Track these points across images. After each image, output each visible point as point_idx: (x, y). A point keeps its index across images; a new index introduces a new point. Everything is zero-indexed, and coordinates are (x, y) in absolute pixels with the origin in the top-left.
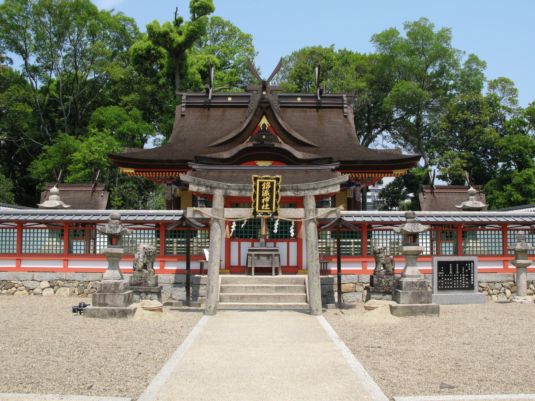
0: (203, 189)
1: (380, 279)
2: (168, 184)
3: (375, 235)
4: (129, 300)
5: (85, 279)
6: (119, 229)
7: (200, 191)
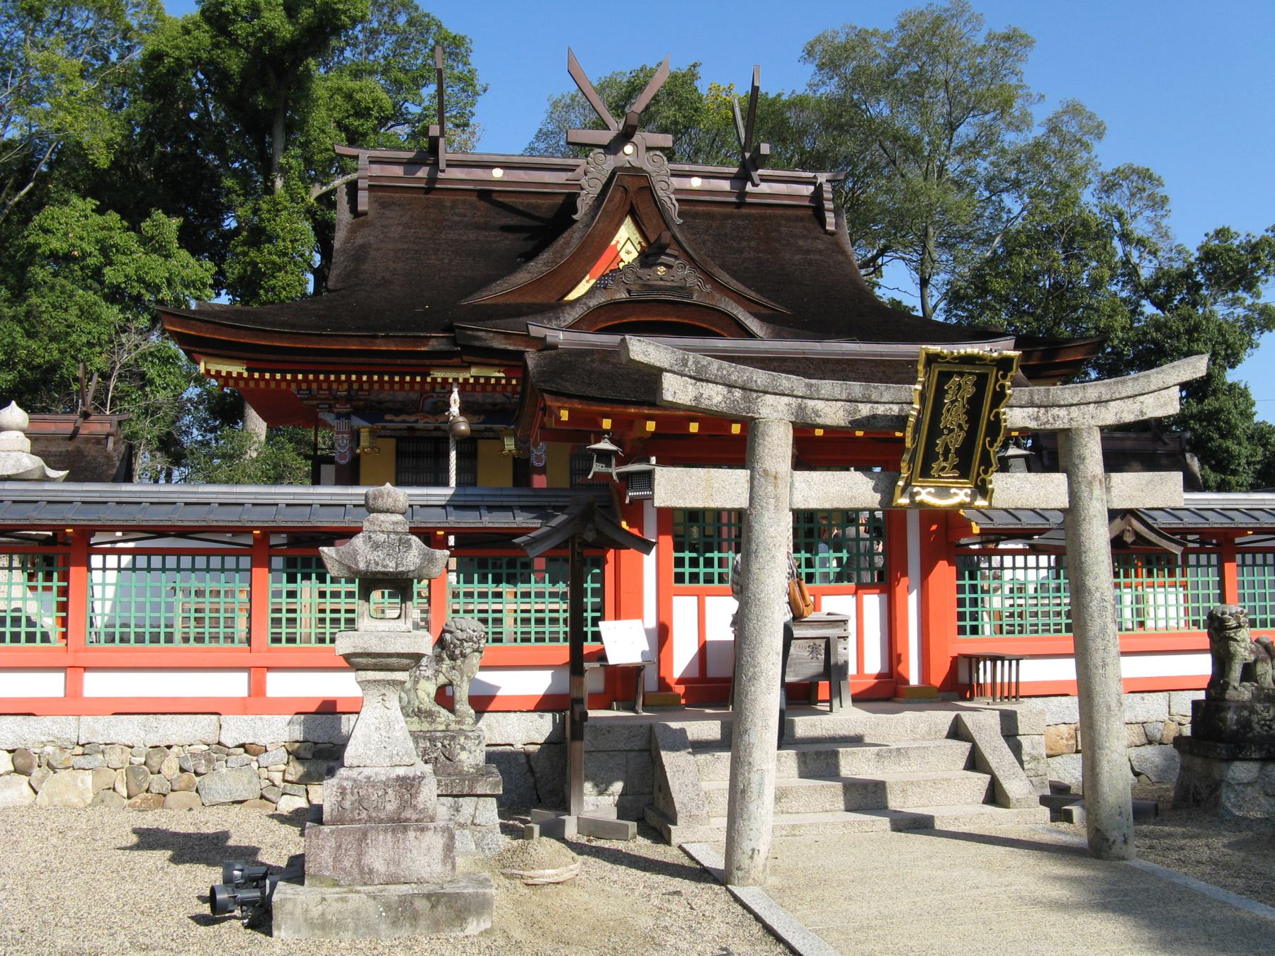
7: (705, 403)
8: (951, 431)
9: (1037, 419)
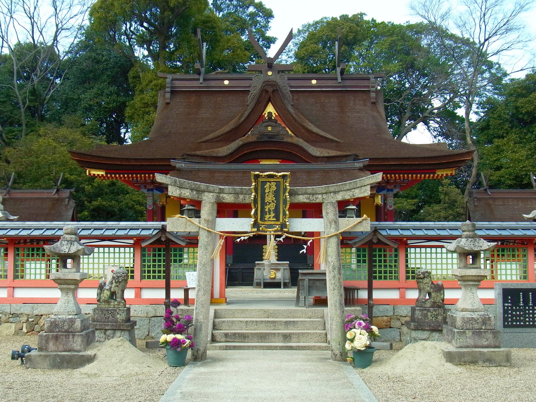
0: (187, 193)
1: (425, 312)
2: (148, 190)
3: (501, 269)
4: (89, 340)
5: (36, 312)
6: (75, 247)
8: (270, 203)
9: (309, 199)
